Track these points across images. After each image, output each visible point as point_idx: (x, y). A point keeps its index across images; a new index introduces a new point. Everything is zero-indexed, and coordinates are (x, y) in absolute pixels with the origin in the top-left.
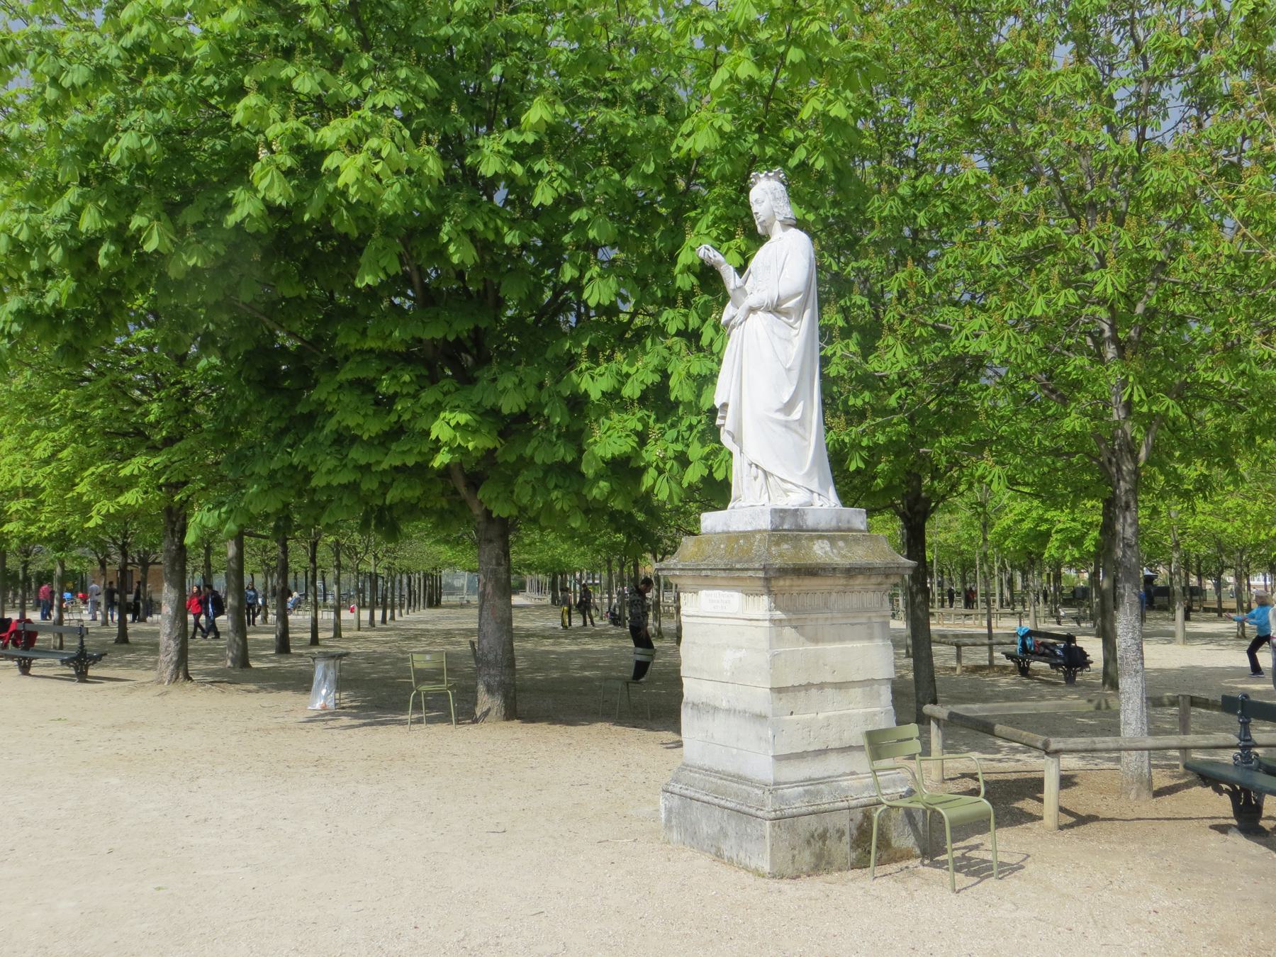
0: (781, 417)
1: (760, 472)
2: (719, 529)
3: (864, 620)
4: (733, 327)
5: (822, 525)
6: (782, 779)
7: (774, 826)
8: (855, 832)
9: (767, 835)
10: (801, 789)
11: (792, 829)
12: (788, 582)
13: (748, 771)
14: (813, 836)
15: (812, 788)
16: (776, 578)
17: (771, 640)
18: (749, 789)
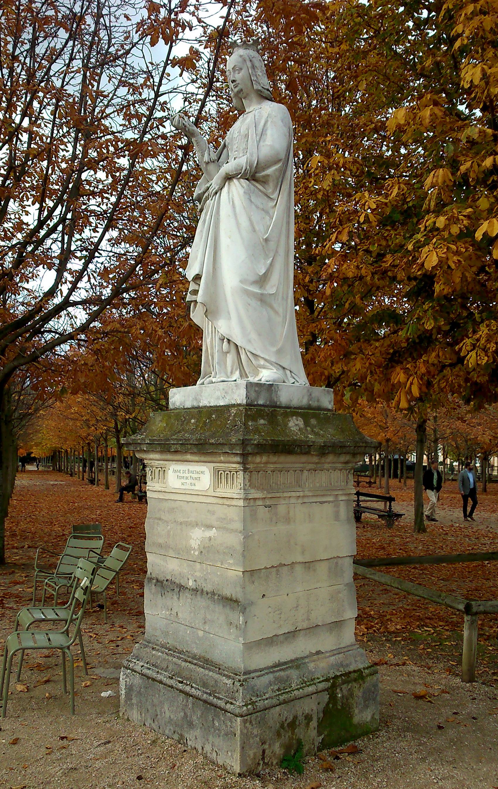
0: (256, 290)
1: (233, 348)
2: (188, 405)
3: (331, 499)
4: (207, 199)
5: (295, 402)
6: (253, 667)
7: (245, 722)
8: (321, 715)
9: (238, 733)
10: (271, 676)
11: (262, 722)
12: (264, 459)
13: (217, 656)
14: (282, 726)
15: (282, 673)
16: (254, 454)
17: (244, 521)
18: (216, 676)
